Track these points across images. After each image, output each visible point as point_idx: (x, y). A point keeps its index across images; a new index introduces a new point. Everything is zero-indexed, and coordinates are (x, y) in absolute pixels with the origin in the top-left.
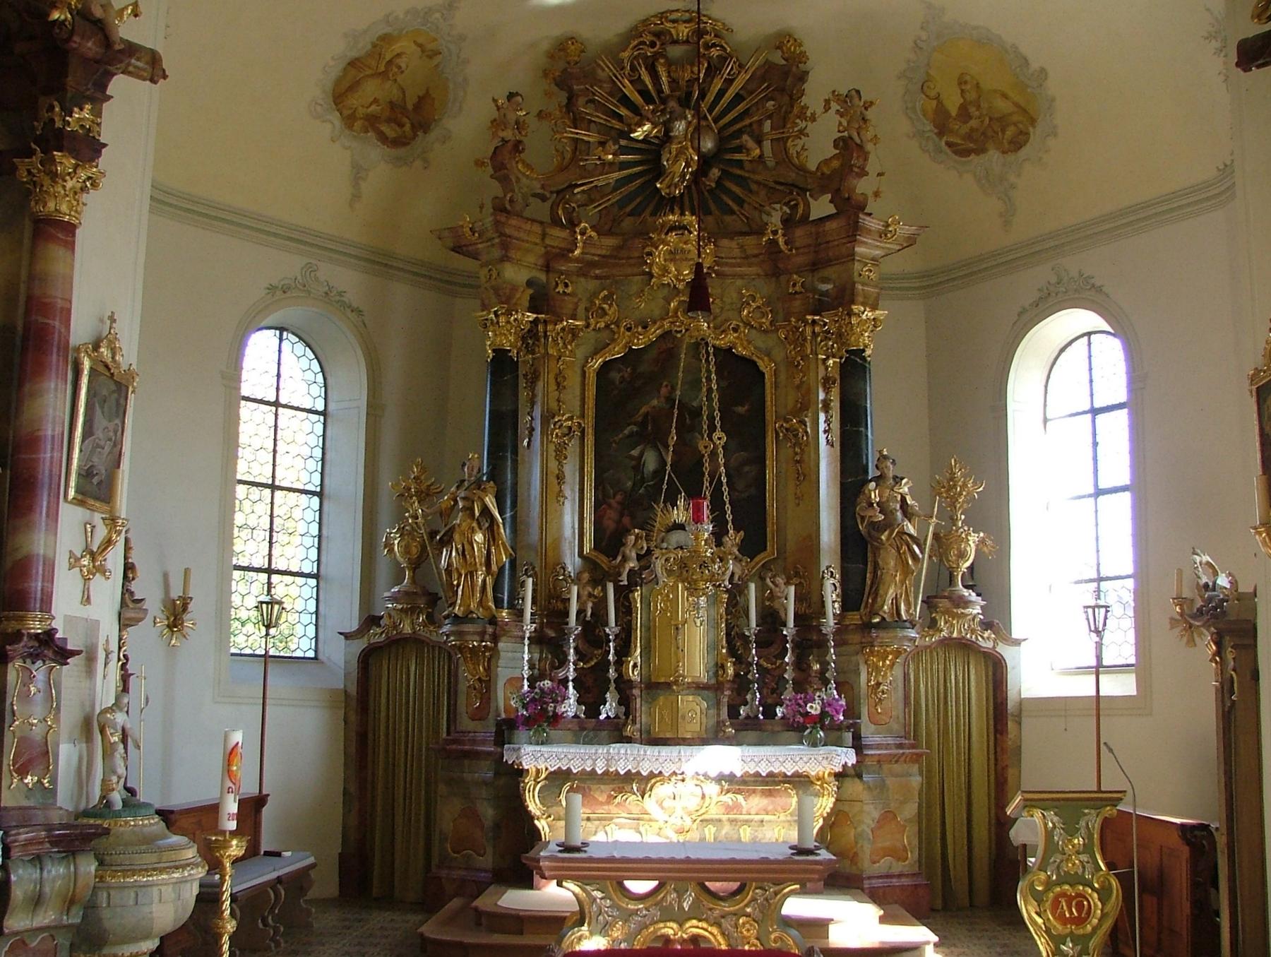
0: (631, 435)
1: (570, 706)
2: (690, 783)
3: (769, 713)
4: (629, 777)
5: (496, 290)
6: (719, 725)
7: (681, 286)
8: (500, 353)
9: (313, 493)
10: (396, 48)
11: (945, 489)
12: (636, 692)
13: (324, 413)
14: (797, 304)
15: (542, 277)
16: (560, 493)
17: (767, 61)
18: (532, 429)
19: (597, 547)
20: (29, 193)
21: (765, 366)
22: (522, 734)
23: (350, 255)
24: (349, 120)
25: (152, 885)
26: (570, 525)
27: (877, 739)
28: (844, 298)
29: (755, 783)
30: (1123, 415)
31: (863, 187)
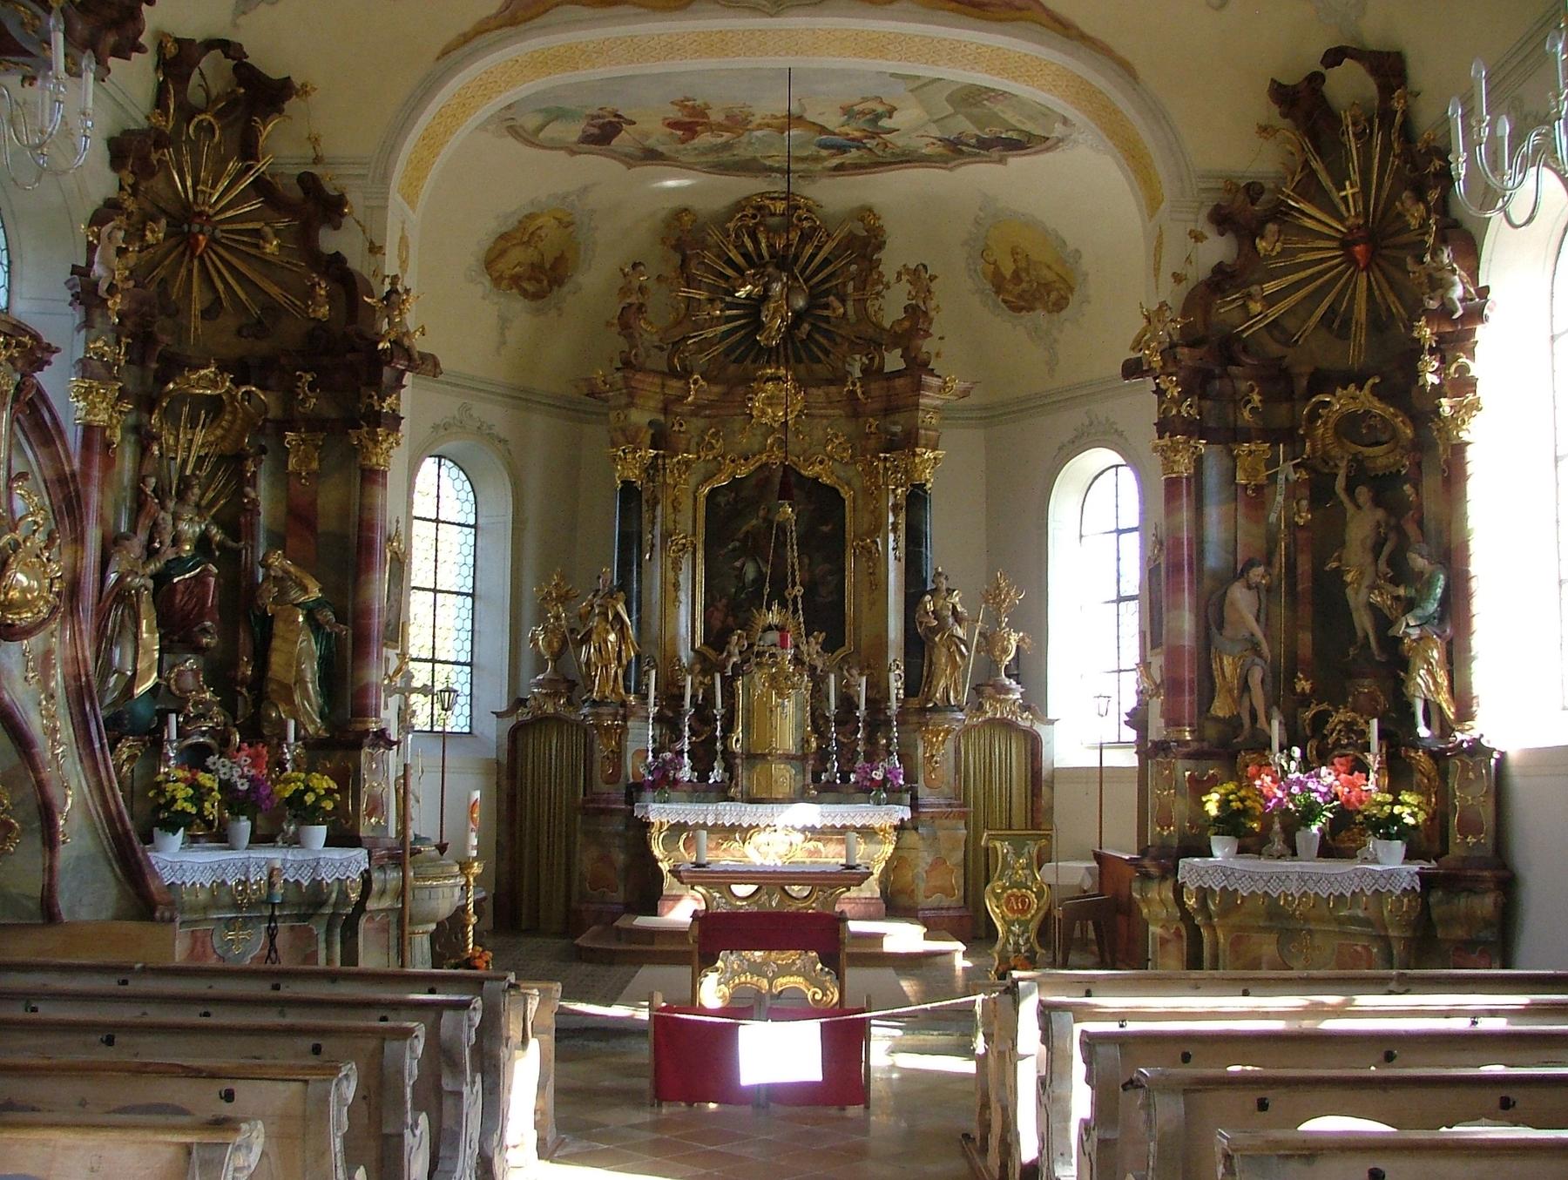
0: (734, 550)
1: (686, 773)
2: (781, 833)
3: (845, 779)
4: (733, 828)
5: (623, 431)
6: (805, 789)
7: (776, 425)
8: (627, 484)
9: (467, 595)
10: (539, 222)
11: (993, 596)
12: (738, 761)
13: (475, 526)
14: (872, 443)
15: (662, 418)
16: (676, 599)
17: (851, 232)
18: (653, 546)
19: (706, 643)
20: (355, 452)
21: (847, 494)
22: (648, 795)
23: (493, 393)
24: (497, 281)
25: (432, 887)
26: (685, 623)
27: (932, 800)
28: (907, 442)
29: (832, 833)
30: (1136, 535)
31: (928, 346)
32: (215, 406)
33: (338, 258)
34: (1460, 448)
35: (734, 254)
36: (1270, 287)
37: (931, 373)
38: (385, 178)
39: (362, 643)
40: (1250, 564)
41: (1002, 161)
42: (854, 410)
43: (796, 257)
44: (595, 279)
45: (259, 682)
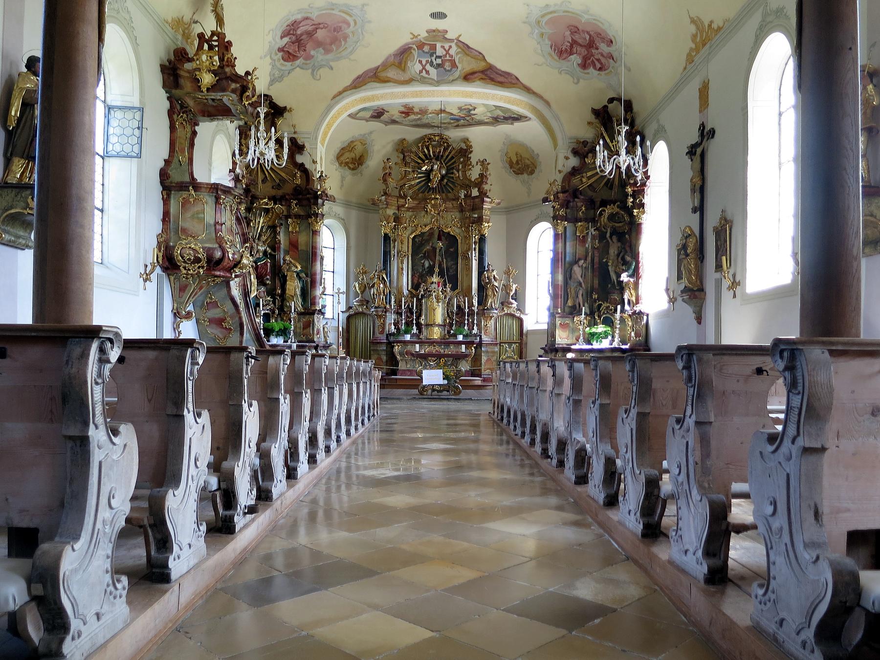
8: (386, 235)
24: (340, 164)
26: (405, 282)
28: (480, 220)
32: (267, 211)
33: (302, 165)
34: (640, 224)
35: (421, 155)
36: (589, 174)
37: (488, 197)
38: (316, 138)
39: (313, 283)
40: (580, 259)
41: (512, 124)
42: (462, 210)
43: (442, 156)
44: (374, 163)
45: (283, 295)
